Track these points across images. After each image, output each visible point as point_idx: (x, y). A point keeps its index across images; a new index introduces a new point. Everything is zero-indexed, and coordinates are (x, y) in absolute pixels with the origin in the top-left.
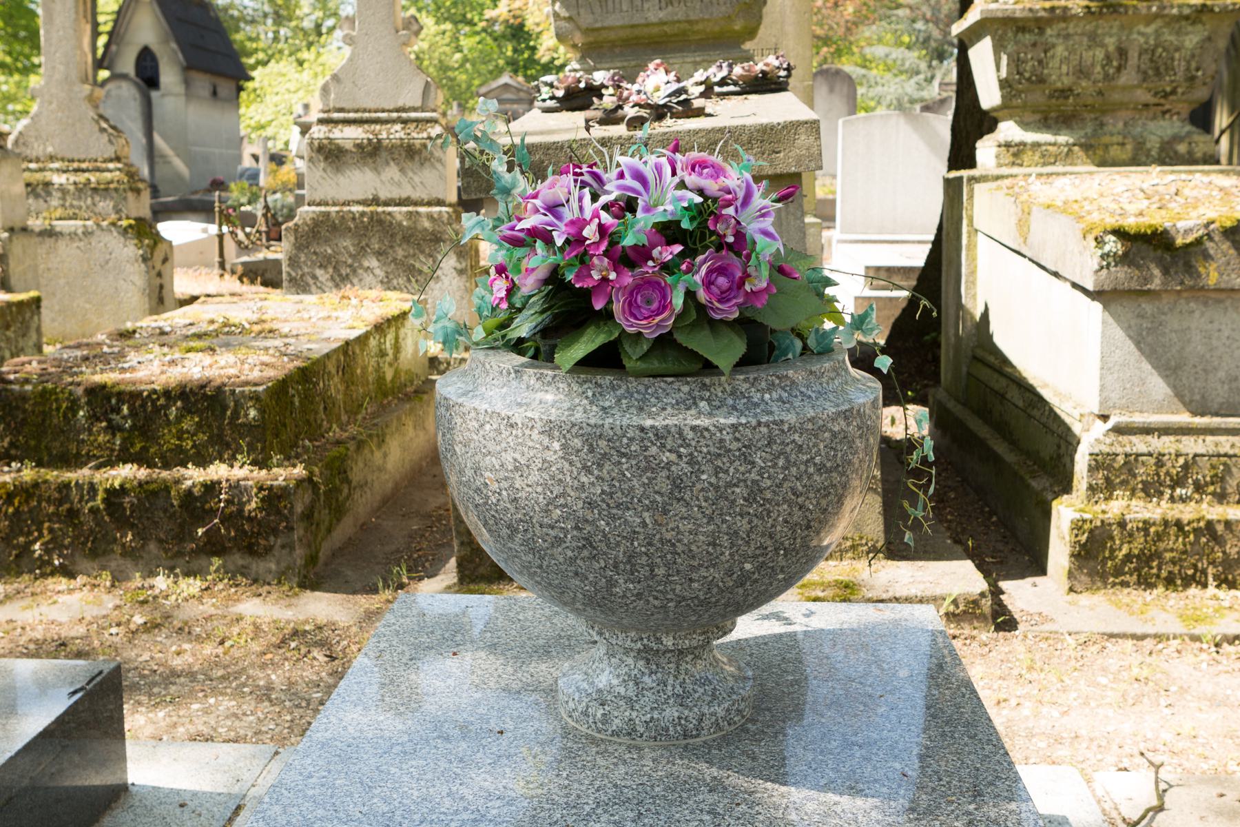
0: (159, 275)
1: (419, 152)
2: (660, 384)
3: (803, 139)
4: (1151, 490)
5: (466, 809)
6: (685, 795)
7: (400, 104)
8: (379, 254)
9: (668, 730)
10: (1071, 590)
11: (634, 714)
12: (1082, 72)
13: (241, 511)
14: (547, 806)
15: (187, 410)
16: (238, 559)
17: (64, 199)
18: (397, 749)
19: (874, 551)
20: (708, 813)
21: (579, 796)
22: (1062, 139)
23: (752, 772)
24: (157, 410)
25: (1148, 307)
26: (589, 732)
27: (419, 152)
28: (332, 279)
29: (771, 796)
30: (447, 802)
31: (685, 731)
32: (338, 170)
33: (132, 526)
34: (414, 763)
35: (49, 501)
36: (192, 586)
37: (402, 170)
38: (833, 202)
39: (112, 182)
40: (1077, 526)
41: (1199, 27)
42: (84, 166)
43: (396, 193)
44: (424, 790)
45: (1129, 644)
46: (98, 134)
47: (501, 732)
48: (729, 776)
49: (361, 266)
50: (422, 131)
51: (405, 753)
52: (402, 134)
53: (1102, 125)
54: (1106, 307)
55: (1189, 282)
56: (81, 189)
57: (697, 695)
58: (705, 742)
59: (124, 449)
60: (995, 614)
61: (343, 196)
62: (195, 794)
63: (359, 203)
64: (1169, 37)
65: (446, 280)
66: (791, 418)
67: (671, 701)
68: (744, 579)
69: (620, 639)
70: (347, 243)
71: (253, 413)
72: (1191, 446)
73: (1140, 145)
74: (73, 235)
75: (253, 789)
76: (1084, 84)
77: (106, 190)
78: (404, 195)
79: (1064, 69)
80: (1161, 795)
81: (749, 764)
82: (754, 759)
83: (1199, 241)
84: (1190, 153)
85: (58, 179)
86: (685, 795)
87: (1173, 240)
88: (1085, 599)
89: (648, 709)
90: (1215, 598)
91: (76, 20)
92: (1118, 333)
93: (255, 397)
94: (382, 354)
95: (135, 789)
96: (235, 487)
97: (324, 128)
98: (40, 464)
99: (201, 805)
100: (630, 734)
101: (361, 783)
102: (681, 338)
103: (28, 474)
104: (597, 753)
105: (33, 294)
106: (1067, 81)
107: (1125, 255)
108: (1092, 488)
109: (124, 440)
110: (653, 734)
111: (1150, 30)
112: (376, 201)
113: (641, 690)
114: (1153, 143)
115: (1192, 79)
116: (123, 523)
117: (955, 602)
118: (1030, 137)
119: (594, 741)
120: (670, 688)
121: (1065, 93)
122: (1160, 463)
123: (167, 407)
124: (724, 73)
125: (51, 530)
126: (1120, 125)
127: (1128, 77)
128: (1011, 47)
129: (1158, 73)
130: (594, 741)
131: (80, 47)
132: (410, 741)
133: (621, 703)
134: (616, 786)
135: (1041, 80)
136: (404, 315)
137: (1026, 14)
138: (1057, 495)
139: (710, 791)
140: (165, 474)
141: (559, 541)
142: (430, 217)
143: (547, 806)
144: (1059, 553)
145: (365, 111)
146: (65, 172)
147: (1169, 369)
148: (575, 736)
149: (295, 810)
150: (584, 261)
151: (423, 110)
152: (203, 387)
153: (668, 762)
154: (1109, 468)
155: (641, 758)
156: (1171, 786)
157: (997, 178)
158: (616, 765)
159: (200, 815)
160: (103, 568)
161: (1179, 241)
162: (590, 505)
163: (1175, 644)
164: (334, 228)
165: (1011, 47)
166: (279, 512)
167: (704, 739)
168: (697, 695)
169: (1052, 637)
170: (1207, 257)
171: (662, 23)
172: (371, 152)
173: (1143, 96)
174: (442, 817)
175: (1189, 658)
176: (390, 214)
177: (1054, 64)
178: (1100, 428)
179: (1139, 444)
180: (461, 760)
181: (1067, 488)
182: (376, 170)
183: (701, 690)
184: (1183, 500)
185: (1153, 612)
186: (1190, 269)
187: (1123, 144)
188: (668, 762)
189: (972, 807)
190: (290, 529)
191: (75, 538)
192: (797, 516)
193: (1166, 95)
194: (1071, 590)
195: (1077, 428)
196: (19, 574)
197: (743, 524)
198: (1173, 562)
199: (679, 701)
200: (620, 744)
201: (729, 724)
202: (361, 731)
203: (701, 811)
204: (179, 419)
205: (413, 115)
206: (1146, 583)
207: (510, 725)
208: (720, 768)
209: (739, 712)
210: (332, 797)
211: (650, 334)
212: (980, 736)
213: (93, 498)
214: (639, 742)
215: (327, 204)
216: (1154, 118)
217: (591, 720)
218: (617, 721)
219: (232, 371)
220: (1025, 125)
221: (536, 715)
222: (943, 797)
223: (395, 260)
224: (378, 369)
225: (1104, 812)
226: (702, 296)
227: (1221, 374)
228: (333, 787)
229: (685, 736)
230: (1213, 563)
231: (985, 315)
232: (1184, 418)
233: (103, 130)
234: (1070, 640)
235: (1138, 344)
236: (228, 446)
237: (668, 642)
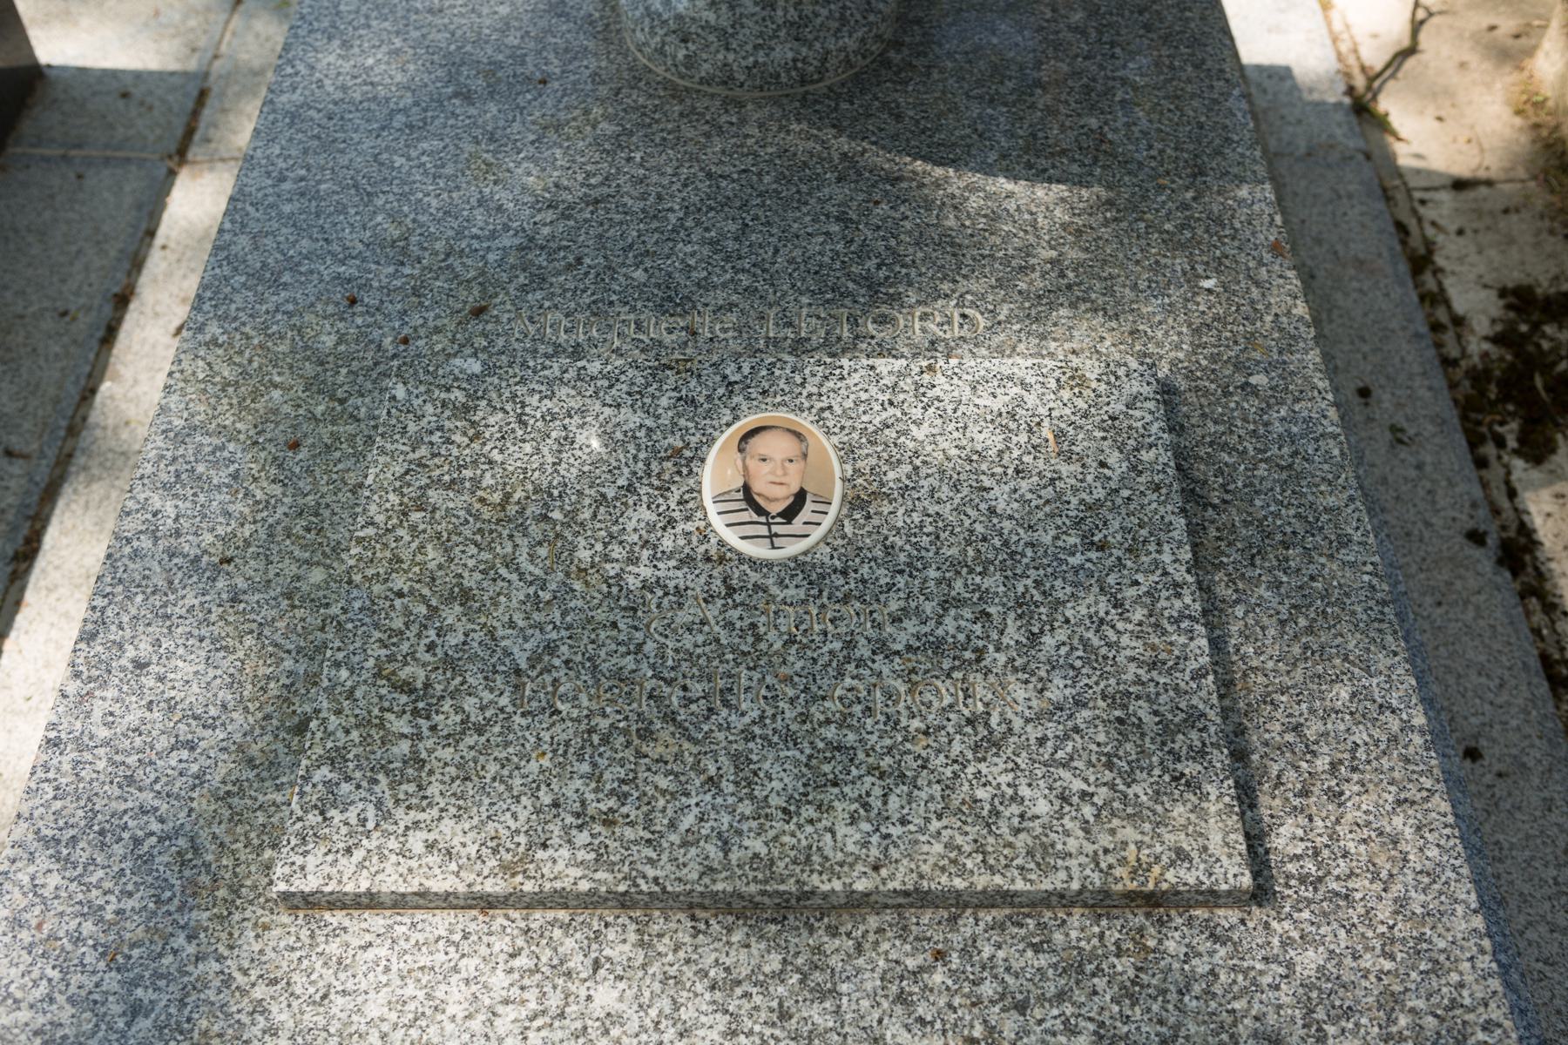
5: (506, 228)
6: (804, 188)
9: (778, 76)
11: (731, 57)
14: (617, 218)
18: (400, 120)
20: (838, 219)
21: (660, 197)
23: (897, 144)
26: (668, 75)
29: (921, 186)
30: (479, 216)
31: (802, 76)
34: (425, 145)
44: (445, 196)
47: (544, 82)
48: (865, 151)
51: (411, 127)
57: (819, 21)
58: (830, 88)
62: (138, 76)
67: (782, 33)
75: (217, 64)
80: (1416, 27)
81: (892, 127)
82: (899, 117)
86: (804, 188)
89: (749, 47)
95: (53, 73)
99: (150, 93)
100: (725, 83)
101: (356, 186)
104: (681, 115)
110: (758, 82)
119: (676, 93)
120: (780, 13)
130: (676, 93)
132: (416, 104)
133: (712, 38)
134: (709, 175)
139: (839, 180)
143: (617, 218)
148: (648, 83)
149: (269, 242)
153: (781, 128)
155: (743, 121)
156: (1431, 15)
158: (707, 135)
159: (150, 108)
167: (828, 83)
168: (819, 21)
174: (476, 244)
180: (492, 139)
183: (824, 12)
188: (781, 128)
189: (1189, 195)
199: (793, 32)
200: (713, 96)
201: (864, 57)
202: (344, 88)
203: (827, 216)
207: (555, 68)
208: (851, 137)
209: (878, 37)
210: (318, 216)
212: (1209, 64)
214: (738, 92)
217: (669, 62)
218: (706, 66)
221: (591, 44)
222: (1153, 178)
225: (1340, 57)
228: (317, 197)
229: (803, 82)
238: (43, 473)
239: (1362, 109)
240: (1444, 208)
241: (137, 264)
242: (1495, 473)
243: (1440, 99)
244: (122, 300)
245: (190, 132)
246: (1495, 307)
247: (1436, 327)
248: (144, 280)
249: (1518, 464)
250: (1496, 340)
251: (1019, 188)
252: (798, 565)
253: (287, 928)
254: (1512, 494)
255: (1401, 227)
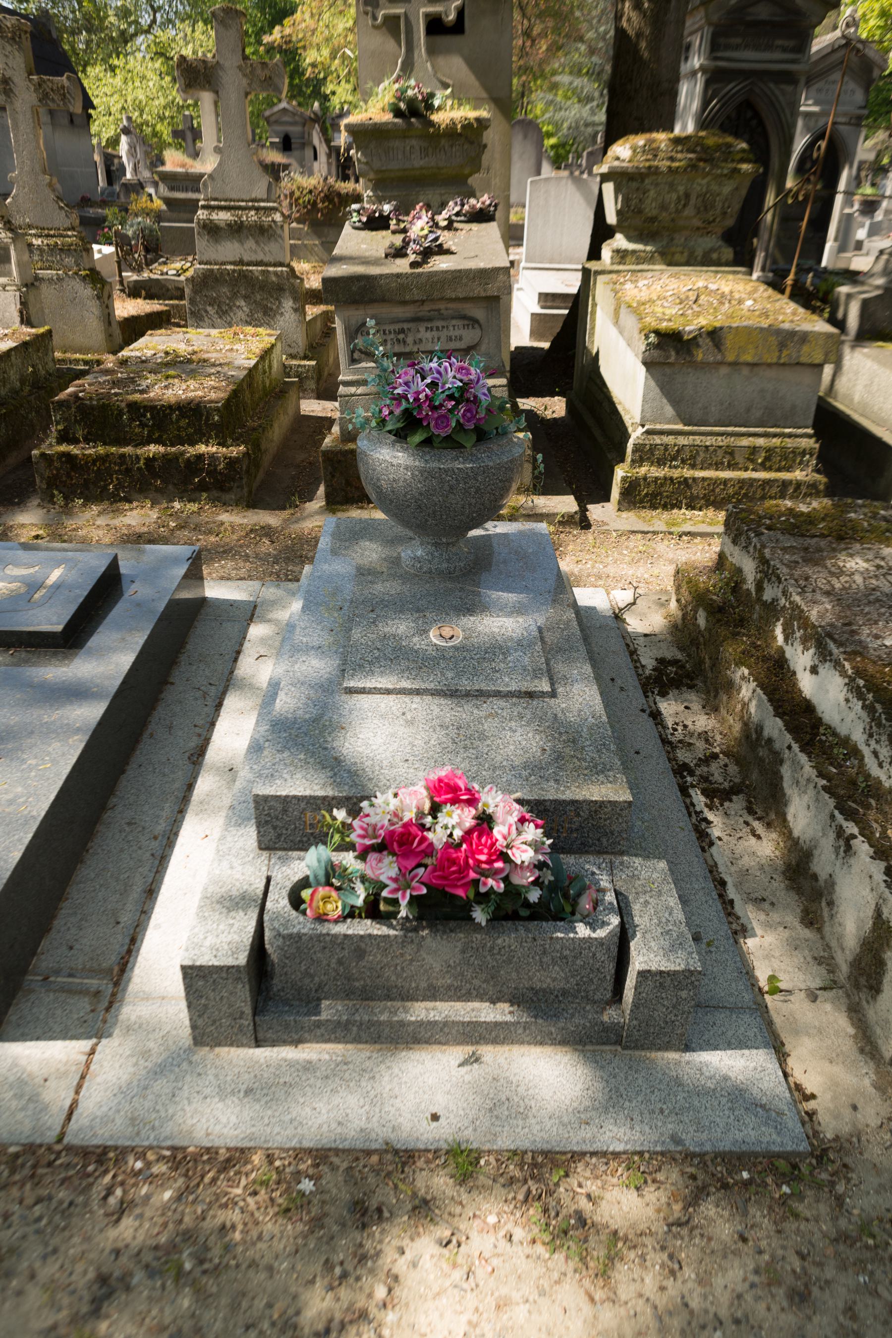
0: (107, 307)
1: (267, 230)
2: (446, 451)
3: (501, 277)
4: (661, 463)
7: (253, 196)
8: (246, 297)
10: (619, 510)
12: (663, 207)
13: (216, 469)
15: (182, 415)
16: (215, 493)
17: (42, 255)
19: (528, 490)
22: (649, 248)
24: (165, 416)
25: (668, 371)
27: (267, 230)
28: (217, 313)
32: (217, 241)
33: (160, 477)
35: (115, 463)
36: (193, 507)
37: (257, 242)
38: (522, 226)
39: (72, 245)
40: (624, 479)
41: (732, 181)
42: (52, 232)
43: (254, 258)
45: (639, 536)
46: (58, 211)
49: (235, 305)
50: (268, 216)
52: (255, 218)
53: (672, 239)
54: (648, 370)
55: (688, 359)
56: (53, 249)
59: (149, 436)
60: (581, 521)
61: (221, 259)
63: (231, 263)
64: (714, 187)
65: (287, 315)
66: (491, 464)
68: (473, 519)
69: (426, 539)
70: (225, 290)
71: (216, 418)
72: (682, 441)
73: (692, 254)
74: (51, 280)
76: (664, 214)
77: (69, 250)
78: (259, 259)
79: (654, 205)
80: (635, 600)
83: (695, 338)
84: (719, 259)
85: (37, 242)
87: (682, 337)
88: (625, 515)
90: (684, 514)
91: (34, 127)
92: (652, 383)
93: (217, 410)
94: (265, 372)
96: (212, 456)
97: (206, 212)
98: (105, 444)
102: (453, 436)
103: (101, 450)
105: (47, 328)
106: (654, 212)
107: (659, 344)
108: (633, 461)
109: (149, 432)
111: (705, 181)
112: (241, 262)
113: (433, 557)
114: (699, 252)
115: (725, 213)
116: (156, 476)
117: (563, 516)
118: (631, 246)
121: (653, 220)
122: (666, 449)
123: (171, 414)
124: (457, 209)
125: (117, 479)
126: (683, 239)
127: (689, 211)
128: (624, 190)
129: (706, 209)
131: (38, 147)
135: (640, 212)
136: (273, 346)
137: (634, 170)
138: (618, 463)
140: (173, 449)
141: (409, 506)
142: (276, 273)
144: (615, 493)
145: (231, 200)
146: (40, 236)
147: (675, 402)
150: (420, 407)
151: (268, 201)
152: (189, 404)
154: (642, 451)
157: (611, 272)
160: (146, 498)
161: (686, 337)
162: (421, 494)
163: (661, 535)
164: (216, 280)
165: (624, 190)
166: (235, 470)
169: (607, 532)
170: (698, 346)
171: (422, 168)
172: (237, 230)
173: (697, 223)
175: (666, 542)
176: (251, 271)
177: (648, 201)
178: (640, 430)
179: (657, 440)
181: (622, 460)
182: (241, 242)
184: (676, 467)
185: (655, 521)
186: (689, 352)
187: (682, 253)
190: (241, 478)
191: (130, 483)
192: (492, 497)
193: (710, 223)
194: (619, 510)
195: (630, 430)
196: (102, 501)
197: (473, 501)
198: (667, 497)
204: (178, 420)
205: (262, 204)
206: (654, 507)
211: (443, 435)
213: (138, 463)
215: (211, 264)
216: (702, 236)
219: (200, 393)
220: (630, 239)
223: (255, 301)
224: (263, 382)
226: (461, 421)
227: (700, 405)
230: (685, 498)
231: (597, 353)
232: (680, 427)
233: (61, 208)
234: (614, 534)
235: (661, 389)
236: (204, 435)
237: (444, 540)
238: (221, 689)
239: (618, 617)
240: (641, 641)
241: (242, 645)
242: (651, 699)
243: (642, 617)
244: (238, 653)
245: (253, 615)
246: (654, 663)
247: (636, 667)
248: (244, 647)
249: (658, 698)
250: (653, 670)
251: (505, 594)
252: (455, 648)
253: (345, 697)
254: (655, 703)
255: (628, 645)
